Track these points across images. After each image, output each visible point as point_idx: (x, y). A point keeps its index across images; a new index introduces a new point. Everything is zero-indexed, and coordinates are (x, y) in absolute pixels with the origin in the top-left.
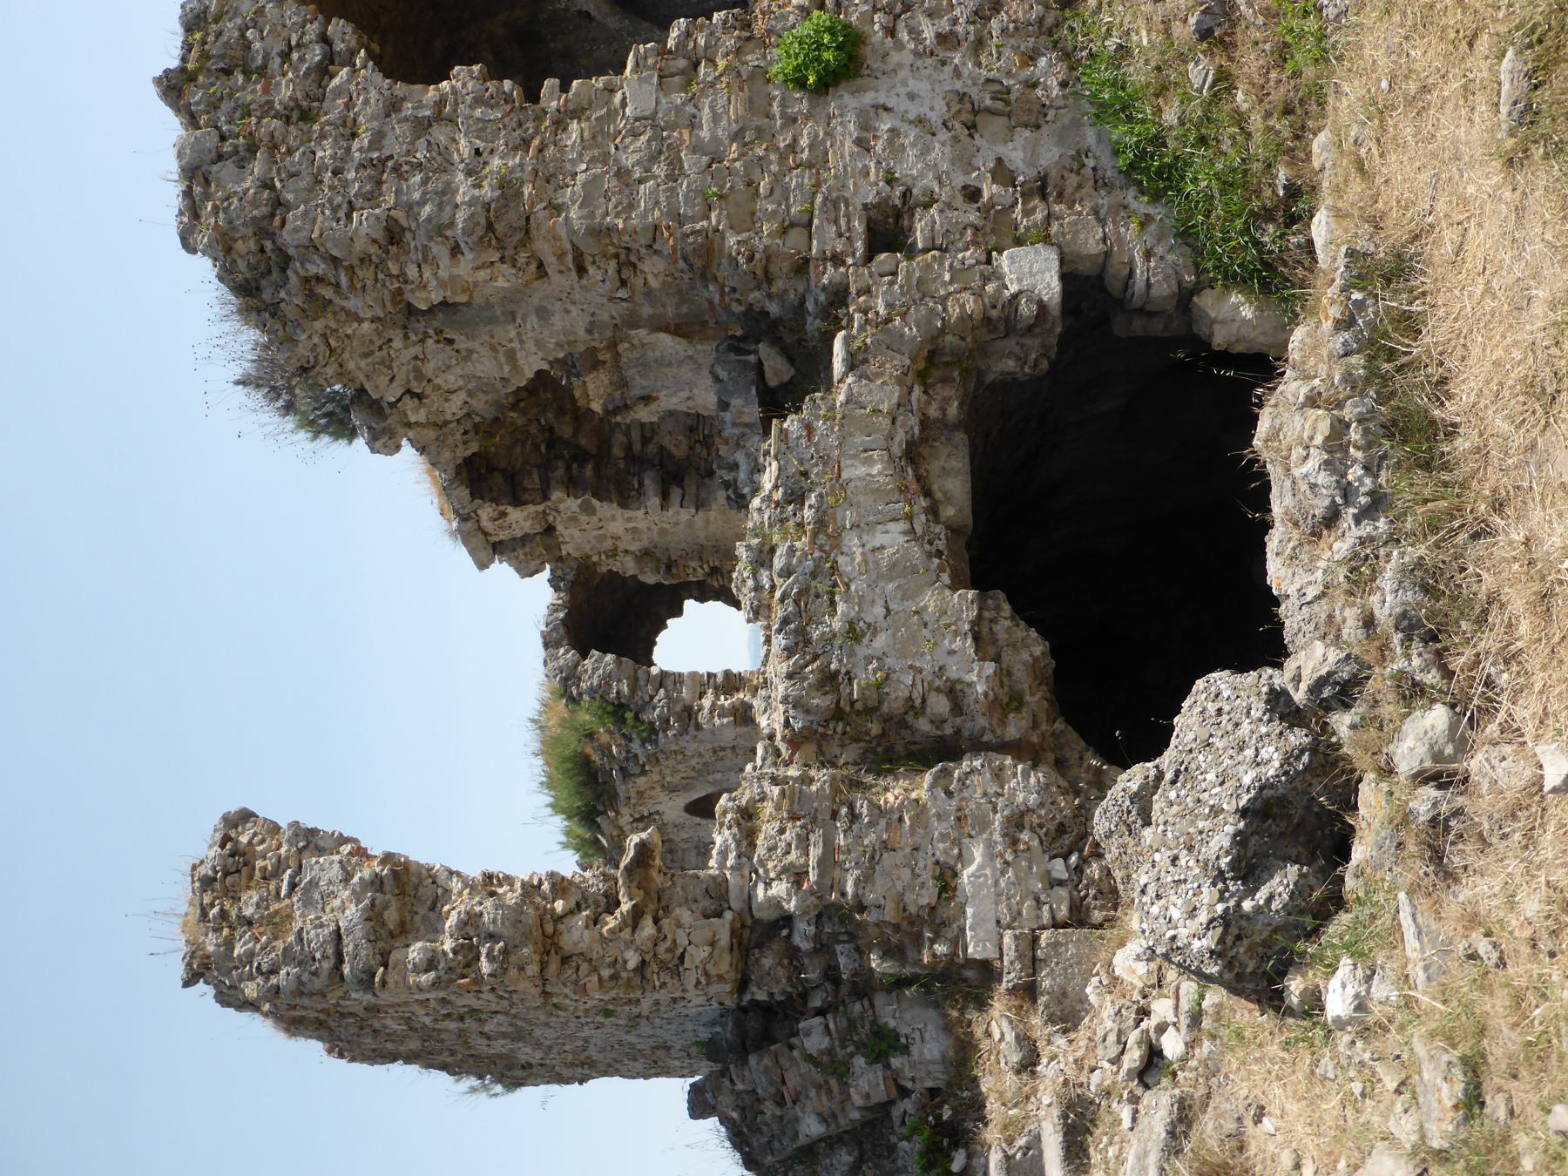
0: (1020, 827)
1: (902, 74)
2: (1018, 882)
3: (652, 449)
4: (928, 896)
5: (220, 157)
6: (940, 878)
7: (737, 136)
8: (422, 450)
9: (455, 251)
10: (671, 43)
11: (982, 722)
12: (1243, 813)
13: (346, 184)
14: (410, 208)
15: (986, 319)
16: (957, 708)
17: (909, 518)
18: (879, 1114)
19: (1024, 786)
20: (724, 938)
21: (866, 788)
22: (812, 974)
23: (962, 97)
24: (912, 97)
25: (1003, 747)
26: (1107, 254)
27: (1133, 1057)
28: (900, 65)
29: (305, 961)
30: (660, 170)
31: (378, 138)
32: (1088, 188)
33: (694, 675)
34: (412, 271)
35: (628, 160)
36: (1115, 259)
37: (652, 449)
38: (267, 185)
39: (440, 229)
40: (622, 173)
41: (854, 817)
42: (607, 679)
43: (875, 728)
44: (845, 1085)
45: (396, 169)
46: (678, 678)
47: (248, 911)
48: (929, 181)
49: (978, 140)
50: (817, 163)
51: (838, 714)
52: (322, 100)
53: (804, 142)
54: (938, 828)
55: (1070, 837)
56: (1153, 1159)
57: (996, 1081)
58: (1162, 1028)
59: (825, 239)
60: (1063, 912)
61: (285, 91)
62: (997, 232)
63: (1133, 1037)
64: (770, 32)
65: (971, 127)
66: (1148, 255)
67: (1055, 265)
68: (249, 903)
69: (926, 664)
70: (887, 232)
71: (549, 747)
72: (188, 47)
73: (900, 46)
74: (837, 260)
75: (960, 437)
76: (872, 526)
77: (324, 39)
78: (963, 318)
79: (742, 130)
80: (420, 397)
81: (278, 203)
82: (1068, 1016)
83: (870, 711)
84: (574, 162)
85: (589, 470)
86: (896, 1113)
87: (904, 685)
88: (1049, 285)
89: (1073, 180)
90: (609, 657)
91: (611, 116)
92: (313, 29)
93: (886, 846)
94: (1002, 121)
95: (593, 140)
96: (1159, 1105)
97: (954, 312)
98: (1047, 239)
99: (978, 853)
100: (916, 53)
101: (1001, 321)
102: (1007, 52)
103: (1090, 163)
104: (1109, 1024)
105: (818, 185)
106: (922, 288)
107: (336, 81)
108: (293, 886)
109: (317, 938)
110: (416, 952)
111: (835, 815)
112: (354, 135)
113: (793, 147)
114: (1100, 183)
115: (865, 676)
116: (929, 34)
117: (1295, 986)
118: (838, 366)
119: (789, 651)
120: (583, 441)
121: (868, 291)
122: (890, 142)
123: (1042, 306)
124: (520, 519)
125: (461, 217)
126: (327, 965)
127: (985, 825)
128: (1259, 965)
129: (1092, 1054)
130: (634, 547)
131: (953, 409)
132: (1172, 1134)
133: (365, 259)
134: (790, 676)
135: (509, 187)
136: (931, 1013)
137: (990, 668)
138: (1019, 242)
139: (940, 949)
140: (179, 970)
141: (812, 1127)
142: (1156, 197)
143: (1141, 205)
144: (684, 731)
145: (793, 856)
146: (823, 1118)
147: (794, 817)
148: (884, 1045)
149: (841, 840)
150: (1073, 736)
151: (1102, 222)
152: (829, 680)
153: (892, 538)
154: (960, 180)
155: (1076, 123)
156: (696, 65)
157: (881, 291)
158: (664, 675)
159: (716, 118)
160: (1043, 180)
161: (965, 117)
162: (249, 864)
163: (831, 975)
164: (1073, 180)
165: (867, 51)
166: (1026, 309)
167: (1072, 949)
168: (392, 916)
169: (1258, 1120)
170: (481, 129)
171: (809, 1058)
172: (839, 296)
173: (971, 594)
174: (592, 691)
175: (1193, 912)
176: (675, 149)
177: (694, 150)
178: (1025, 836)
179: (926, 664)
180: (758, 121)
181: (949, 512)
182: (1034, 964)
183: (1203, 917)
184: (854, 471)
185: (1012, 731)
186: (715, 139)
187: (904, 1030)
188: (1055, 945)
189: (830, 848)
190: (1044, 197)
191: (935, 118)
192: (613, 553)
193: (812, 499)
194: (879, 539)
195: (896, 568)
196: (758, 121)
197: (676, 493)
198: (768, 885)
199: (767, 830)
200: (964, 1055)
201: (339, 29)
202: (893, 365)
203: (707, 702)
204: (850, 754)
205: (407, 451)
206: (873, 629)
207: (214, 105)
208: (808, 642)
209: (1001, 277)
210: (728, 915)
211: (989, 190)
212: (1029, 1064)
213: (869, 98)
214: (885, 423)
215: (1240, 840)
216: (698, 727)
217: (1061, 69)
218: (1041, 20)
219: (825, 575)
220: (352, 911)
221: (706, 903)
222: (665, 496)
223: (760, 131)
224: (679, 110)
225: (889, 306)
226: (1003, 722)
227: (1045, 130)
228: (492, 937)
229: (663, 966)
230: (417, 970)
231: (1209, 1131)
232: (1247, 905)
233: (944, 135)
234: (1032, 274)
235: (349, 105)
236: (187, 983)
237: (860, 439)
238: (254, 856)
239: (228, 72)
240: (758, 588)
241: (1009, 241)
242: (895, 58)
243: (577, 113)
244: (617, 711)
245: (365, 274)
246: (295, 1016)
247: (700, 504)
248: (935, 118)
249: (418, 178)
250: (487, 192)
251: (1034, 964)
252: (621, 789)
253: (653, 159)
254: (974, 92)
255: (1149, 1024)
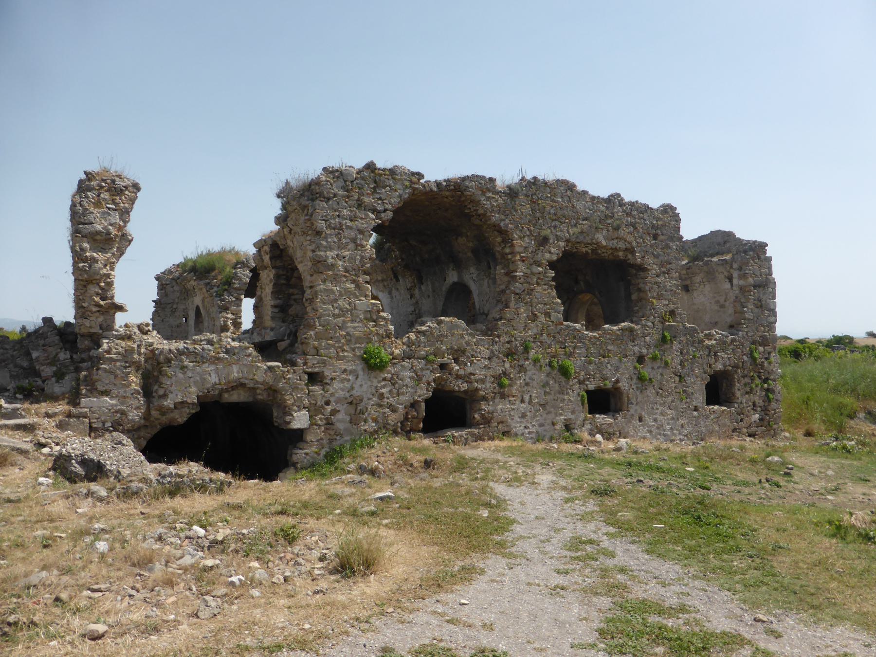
0: (122, 414)
1: (369, 383)
2: (104, 413)
3: (292, 302)
4: (100, 388)
5: (345, 181)
6: (106, 391)
7: (348, 334)
8: (279, 232)
9: (314, 251)
10: (382, 314)
11: (156, 404)
12: (99, 461)
13: (335, 219)
14: (326, 238)
15: (285, 407)
16: (160, 397)
17: (220, 384)
18: (37, 374)
19: (135, 415)
20: (92, 330)
21: (137, 371)
22: (83, 356)
23: (361, 400)
24: (361, 386)
25: (148, 409)
26: (307, 442)
27: (43, 441)
28: (372, 382)
29: (84, 214)
30: (337, 311)
31: (350, 228)
32: (329, 437)
33: (241, 311)
34: (309, 238)
35: (340, 302)
36: (305, 444)
37: (292, 302)
38: (335, 195)
39: (318, 247)
40: (336, 300)
41: (126, 367)
42: (240, 279)
43: (155, 374)
44: (48, 364)
45: (339, 234)
46: (239, 305)
47: (102, 196)
48: (331, 390)
49: (346, 405)
50: (339, 358)
51: (159, 363)
52: (365, 210)
53: (346, 354)
54: (121, 391)
55: (116, 426)
56: (12, 444)
57: (44, 407)
58: (51, 448)
59: (312, 360)
60: (94, 425)
61: (366, 200)
62: (314, 410)
63: (49, 441)
64: (384, 343)
65: (351, 403)
66: (306, 454)
67: (302, 427)
68: (105, 195)
69: (173, 388)
70: (314, 378)
71: (222, 254)
72: (384, 170)
73: (379, 382)
74: (305, 364)
75: (251, 399)
76: (217, 373)
77: (385, 210)
78: (285, 400)
79: (350, 335)
80: (290, 232)
81: (329, 199)
82: (61, 426)
83: (160, 372)
84: (340, 286)
85: (283, 282)
86: (37, 379)
87: (166, 382)
88: (296, 425)
89: (332, 433)
90: (248, 280)
91: (356, 297)
92: (390, 207)
93: (116, 376)
94: (353, 412)
95: (347, 291)
96: (29, 447)
97: (287, 397)
98: (311, 425)
99: (114, 402)
100: (377, 387)
101: (286, 411)
102: (377, 414)
103: (338, 438)
104: (54, 435)
105: (330, 358)
106: (295, 388)
107: (370, 214)
108: (109, 209)
109: (91, 218)
110: (86, 245)
111: (126, 362)
112: (351, 220)
113: (343, 350)
114: (331, 441)
115: (170, 371)
116: (383, 390)
117: (51, 473)
118: (269, 364)
119: (178, 350)
120: (293, 280)
121: (294, 372)
122: (345, 379)
123: (289, 423)
124: (267, 258)
125: (322, 253)
126: (82, 221)
127: (122, 404)
128: (60, 465)
129: (48, 429)
130: (263, 295)
131: (260, 397)
132: (18, 449)
133: (312, 224)
134: (170, 350)
135: (332, 267)
136: (68, 389)
137: (172, 406)
138: (310, 417)
139: (84, 391)
140: (89, 169)
141: (35, 355)
142: (326, 456)
143: (323, 452)
144: (219, 307)
145: (114, 350)
146: (37, 358)
147: (126, 351)
148: (59, 376)
149: (118, 364)
150: (154, 431)
151: (318, 441)
152: (169, 361)
153: (213, 379)
154: (332, 399)
155: (352, 434)
156: (374, 321)
157: (294, 376)
158: (241, 300)
159: (354, 328)
160: (332, 424)
161: (355, 402)
162: (118, 195)
163: (83, 361)
164: (332, 433)
165: (378, 372)
166: (288, 418)
167: (82, 427)
168: (98, 237)
169: (20, 469)
170: (352, 259)
171: (57, 354)
172: (293, 364)
173: (196, 401)
174: (236, 274)
175: (73, 449)
176: (344, 315)
177: (344, 322)
178: (119, 415)
179: (173, 388)
180: (353, 340)
181: (226, 395)
182: (78, 417)
183: (71, 451)
184: (235, 368)
185: (153, 412)
186: (347, 327)
187: (64, 381)
188: (83, 423)
189: (116, 361)
190: (326, 424)
191: (354, 392)
192: (261, 288)
193: (226, 356)
194: (213, 375)
195: (204, 380)
196: (353, 340)
197: (277, 310)
198: (107, 343)
199: (123, 344)
200: (54, 398)
201: (390, 215)
202: (269, 379)
203: (230, 316)
204: (149, 367)
205: (277, 228)
206: (185, 373)
207: (363, 178)
208: (181, 355)
209: (299, 411)
210: (101, 331)
211: (329, 408)
212: (48, 415)
213: (361, 373)
214: (251, 376)
215: (92, 461)
216: (221, 312)
217: (371, 430)
218: (389, 424)
219: (225, 358)
220: (99, 228)
221: (105, 325)
222: (275, 306)
223: (350, 341)
224: (358, 317)
225: (289, 379)
226: (156, 410)
227: (349, 425)
228: (90, 267)
229: (84, 313)
230: (80, 246)
231: (20, 458)
232: (73, 461)
233: (348, 395)
234: (300, 420)
235: (361, 219)
236: (85, 172)
237: (245, 370)
238: (121, 196)
239: (375, 182)
240: (201, 341)
241: (312, 413)
242: (375, 381)
243: (358, 286)
244: (228, 283)
245: (308, 224)
246: (73, 206)
247: (273, 318)
248: (354, 392)
249: (336, 240)
250: (330, 261)
251: (78, 417)
252: (202, 282)
253: (341, 309)
254: (363, 404)
255: (53, 445)
